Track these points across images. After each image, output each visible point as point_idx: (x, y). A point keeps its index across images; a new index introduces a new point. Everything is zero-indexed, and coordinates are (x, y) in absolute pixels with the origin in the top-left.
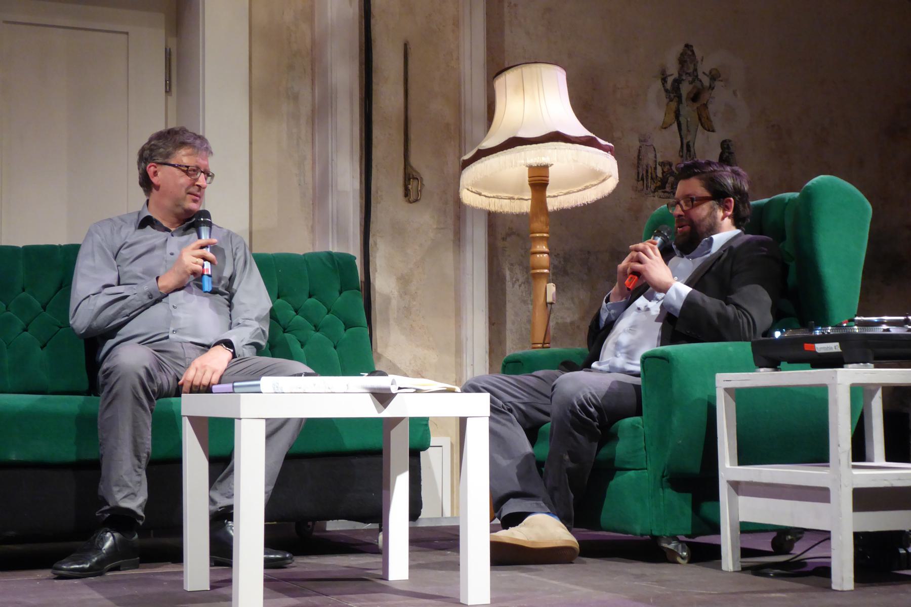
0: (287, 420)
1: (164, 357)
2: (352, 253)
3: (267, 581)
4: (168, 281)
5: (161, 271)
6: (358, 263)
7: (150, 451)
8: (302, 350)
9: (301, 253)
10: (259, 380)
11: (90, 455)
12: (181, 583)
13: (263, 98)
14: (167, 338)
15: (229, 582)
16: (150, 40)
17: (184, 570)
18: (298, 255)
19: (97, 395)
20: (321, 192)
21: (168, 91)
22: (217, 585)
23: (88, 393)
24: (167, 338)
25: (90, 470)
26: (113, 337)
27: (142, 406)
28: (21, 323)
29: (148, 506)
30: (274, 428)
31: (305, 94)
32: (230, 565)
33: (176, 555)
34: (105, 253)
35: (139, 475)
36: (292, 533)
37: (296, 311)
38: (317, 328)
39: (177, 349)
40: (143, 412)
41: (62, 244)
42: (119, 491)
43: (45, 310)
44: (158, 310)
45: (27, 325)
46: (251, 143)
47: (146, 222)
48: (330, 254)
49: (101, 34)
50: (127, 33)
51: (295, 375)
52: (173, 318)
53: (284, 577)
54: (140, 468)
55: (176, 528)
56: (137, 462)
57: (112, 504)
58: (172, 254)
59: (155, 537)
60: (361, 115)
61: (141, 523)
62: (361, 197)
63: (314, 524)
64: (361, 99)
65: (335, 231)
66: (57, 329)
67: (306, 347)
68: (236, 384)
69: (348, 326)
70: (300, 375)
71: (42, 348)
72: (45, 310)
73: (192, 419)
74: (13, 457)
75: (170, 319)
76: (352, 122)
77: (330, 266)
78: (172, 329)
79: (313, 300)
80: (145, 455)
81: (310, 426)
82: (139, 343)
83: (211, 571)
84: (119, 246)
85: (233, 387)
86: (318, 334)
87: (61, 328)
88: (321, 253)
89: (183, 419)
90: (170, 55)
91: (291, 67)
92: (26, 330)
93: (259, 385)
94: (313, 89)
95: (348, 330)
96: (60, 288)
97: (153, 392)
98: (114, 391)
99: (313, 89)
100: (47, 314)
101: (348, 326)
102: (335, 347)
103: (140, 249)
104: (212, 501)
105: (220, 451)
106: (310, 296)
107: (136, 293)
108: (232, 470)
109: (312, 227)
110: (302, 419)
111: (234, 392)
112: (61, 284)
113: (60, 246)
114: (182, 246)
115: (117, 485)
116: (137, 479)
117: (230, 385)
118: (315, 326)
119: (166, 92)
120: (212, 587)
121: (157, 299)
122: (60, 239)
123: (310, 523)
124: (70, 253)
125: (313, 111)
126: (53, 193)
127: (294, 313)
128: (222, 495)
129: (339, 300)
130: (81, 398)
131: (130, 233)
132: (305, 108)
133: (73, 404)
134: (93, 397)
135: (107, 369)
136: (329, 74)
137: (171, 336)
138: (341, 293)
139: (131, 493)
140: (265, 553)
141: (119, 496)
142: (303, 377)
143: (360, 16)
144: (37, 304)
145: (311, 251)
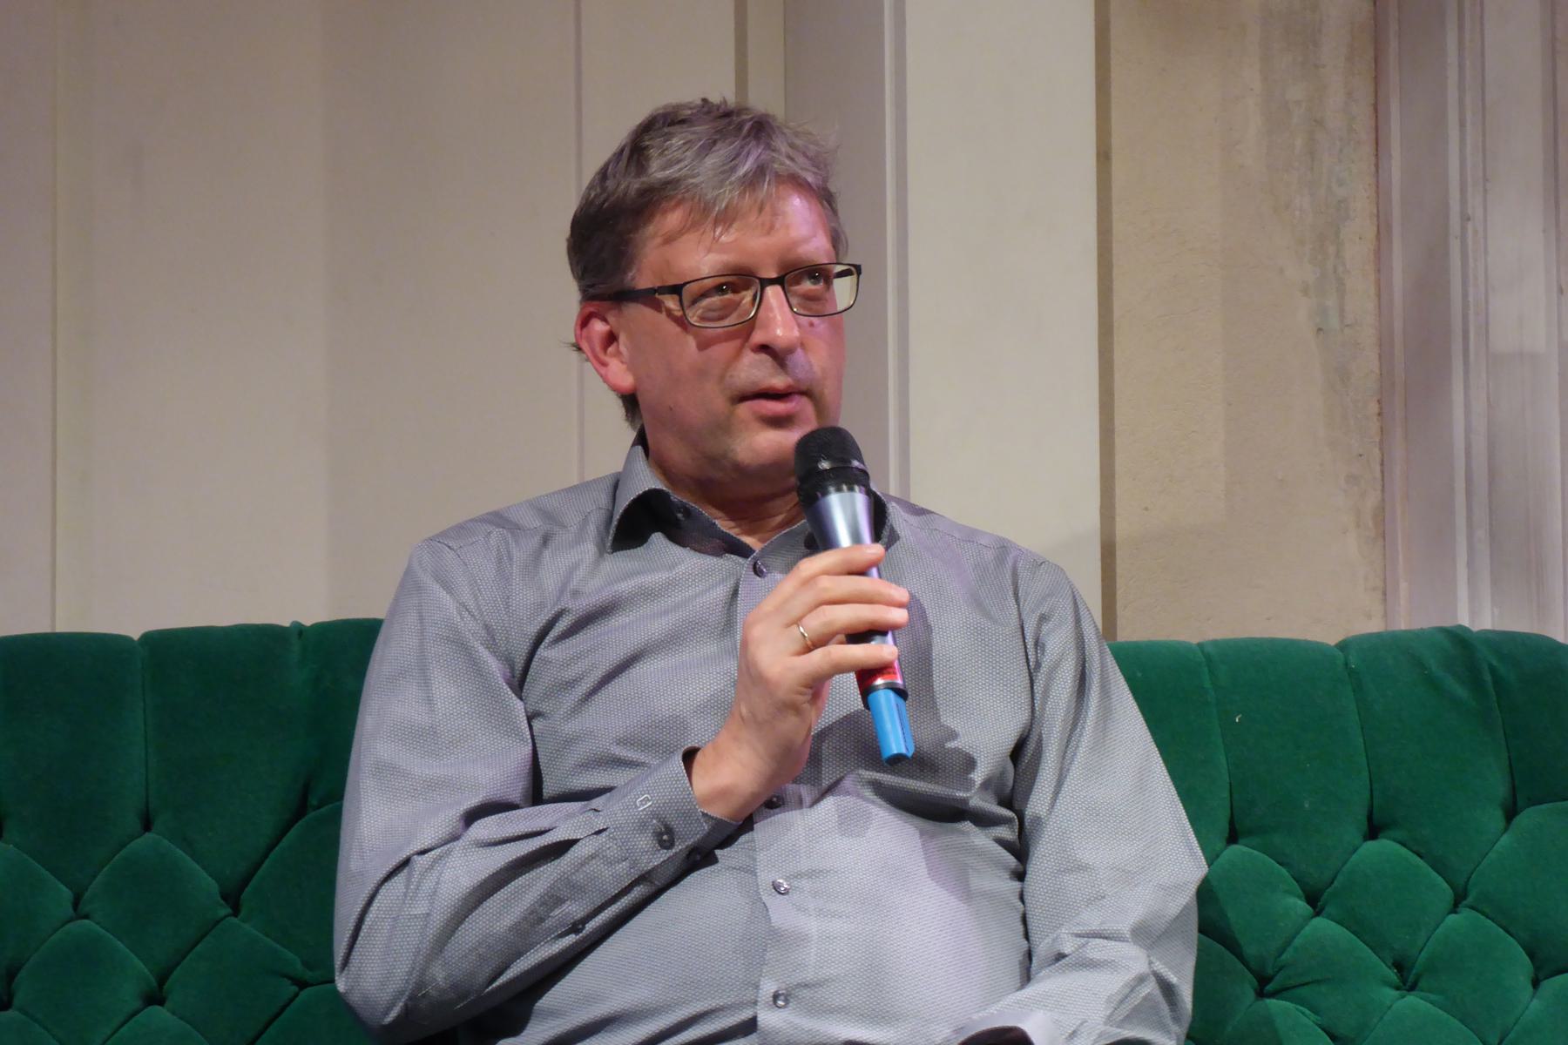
14: (749, 1027)
24: (749, 1027)
28: (137, 970)
37: (1314, 899)
38: (1406, 976)
41: (308, 621)
43: (236, 911)
45: (162, 979)
46: (1104, 156)
48: (1459, 639)
52: (777, 937)
65: (1481, 534)
66: (294, 988)
72: (236, 911)
75: (764, 941)
77: (1461, 691)
78: (768, 987)
79: (1384, 846)
86: (1412, 999)
87: (302, 985)
88: (1419, 635)
92: (154, 998)
96: (301, 811)
106: (1373, 832)
109: (1381, 517)
113: (299, 630)
118: (1400, 966)
121: (701, 848)
122: (298, 599)
124: (344, 652)
127: (1302, 906)
137: (769, 1019)
138: (1511, 813)
144: (209, 885)
145: (1374, 626)
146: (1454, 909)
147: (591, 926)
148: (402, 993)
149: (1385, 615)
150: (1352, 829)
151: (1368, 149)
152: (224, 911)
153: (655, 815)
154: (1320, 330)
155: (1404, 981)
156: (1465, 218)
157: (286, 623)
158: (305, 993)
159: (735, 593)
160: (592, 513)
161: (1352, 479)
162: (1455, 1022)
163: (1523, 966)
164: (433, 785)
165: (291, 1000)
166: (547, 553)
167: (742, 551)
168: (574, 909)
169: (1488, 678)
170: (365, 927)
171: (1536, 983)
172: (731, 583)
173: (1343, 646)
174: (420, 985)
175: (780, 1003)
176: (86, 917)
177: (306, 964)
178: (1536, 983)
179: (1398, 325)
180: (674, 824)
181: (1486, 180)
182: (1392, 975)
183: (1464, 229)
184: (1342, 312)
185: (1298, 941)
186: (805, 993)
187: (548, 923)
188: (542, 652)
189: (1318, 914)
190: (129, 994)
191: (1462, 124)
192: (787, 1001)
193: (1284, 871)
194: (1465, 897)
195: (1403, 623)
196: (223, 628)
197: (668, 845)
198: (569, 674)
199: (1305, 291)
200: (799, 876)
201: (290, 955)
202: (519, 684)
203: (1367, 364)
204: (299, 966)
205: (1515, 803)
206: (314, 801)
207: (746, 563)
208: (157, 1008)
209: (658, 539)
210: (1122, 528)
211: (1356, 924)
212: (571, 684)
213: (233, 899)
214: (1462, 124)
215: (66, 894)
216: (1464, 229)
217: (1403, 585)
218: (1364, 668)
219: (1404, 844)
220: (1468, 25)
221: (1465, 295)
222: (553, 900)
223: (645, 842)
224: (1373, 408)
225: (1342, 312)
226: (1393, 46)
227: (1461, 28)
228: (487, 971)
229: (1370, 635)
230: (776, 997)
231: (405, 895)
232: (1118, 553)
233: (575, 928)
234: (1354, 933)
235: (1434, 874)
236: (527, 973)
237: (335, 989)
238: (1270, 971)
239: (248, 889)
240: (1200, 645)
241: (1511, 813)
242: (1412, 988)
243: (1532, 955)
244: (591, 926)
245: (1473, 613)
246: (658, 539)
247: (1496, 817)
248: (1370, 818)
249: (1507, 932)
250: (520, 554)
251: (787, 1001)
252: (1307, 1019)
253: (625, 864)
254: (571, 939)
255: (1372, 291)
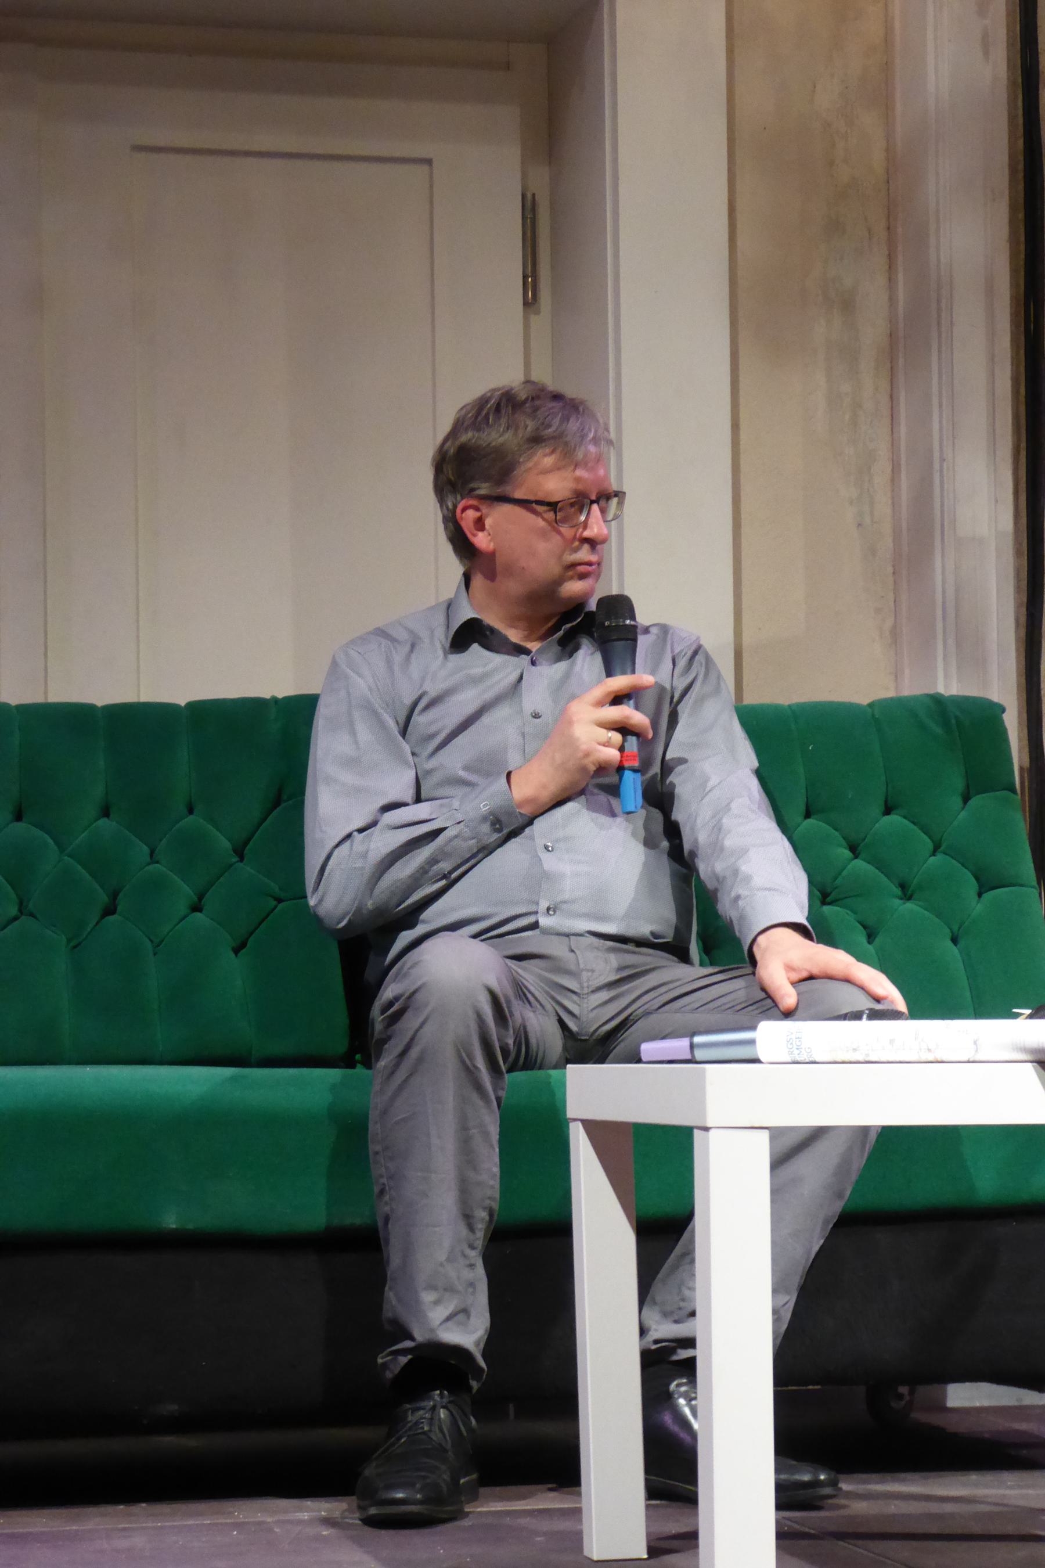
0: (818, 1134)
1: (530, 974)
2: (995, 698)
3: (784, 1536)
4: (532, 783)
5: (513, 760)
6: (1013, 722)
7: (496, 1206)
8: (870, 947)
9: (864, 700)
10: (753, 1028)
11: (354, 1217)
12: (576, 1540)
13: (765, 310)
14: (535, 926)
15: (690, 1539)
16: (480, 173)
17: (584, 1505)
18: (858, 706)
19: (368, 1064)
20: (914, 542)
21: (530, 303)
22: (665, 1544)
23: (347, 1062)
24: (535, 926)
25: (358, 1254)
26: (411, 926)
27: (479, 1087)
28: (186, 892)
29: (493, 1342)
30: (791, 1149)
31: (873, 293)
32: (691, 1500)
33: (561, 1468)
34: (375, 713)
35: (472, 1266)
36: (841, 1415)
37: (854, 849)
38: (906, 892)
39: (556, 948)
40: (480, 1103)
41: (280, 696)
42: (437, 1302)
43: (242, 858)
44: (511, 856)
45: (201, 897)
46: (735, 426)
47: (468, 635)
48: (938, 702)
49: (363, 166)
50: (429, 162)
51: (844, 1017)
52: (547, 876)
53: (832, 1528)
54: (472, 1247)
55: (562, 1399)
56: (464, 1231)
57: (420, 1336)
58: (536, 716)
59: (517, 1420)
60: (1014, 341)
61: (475, 1385)
62: (1018, 553)
63: (912, 1392)
64: (1014, 298)
65: (951, 641)
66: (274, 903)
67: (878, 941)
68: (697, 1039)
69: (985, 884)
70: (857, 1016)
71: (237, 951)
72: (242, 858)
73: (596, 1129)
74: (171, 1221)
75: (539, 879)
76: (992, 359)
77: (939, 730)
78: (544, 905)
79: (894, 818)
80: (484, 1215)
81: (894, 1145)
82: (475, 936)
83: (647, 1507)
84: (408, 701)
85: (692, 1046)
86: (909, 905)
87: (280, 901)
88: (915, 699)
89: (572, 1125)
90: (534, 209)
91: (835, 227)
92: (196, 908)
93: (752, 1042)
94: (891, 280)
95: (988, 896)
96: (277, 803)
97: (505, 1051)
98: (414, 1053)
99: (891, 280)
100: (246, 870)
101: (985, 884)
102: (955, 940)
103: (466, 702)
104: (643, 1331)
105: (661, 1206)
106: (888, 811)
107: (458, 814)
108: (689, 1255)
109: (895, 634)
110: (865, 1130)
111: (692, 1061)
112: (280, 792)
113: (275, 700)
114: (563, 693)
115: (432, 1287)
116: (467, 1274)
117: (685, 1042)
118: (903, 886)
119: (526, 304)
120: (654, 1551)
121: (509, 826)
122: (275, 683)
123: (904, 1390)
124: (300, 712)
125: (892, 335)
126: (234, 573)
127: (847, 853)
128: (666, 1315)
129: (960, 818)
130: (334, 1074)
131: (435, 668)
132: (872, 330)
133: (312, 1088)
134: (360, 1070)
135: (397, 999)
136: (932, 241)
137: (544, 921)
138: (966, 799)
139: (451, 1309)
140: (777, 1470)
141: (437, 1315)
142: (865, 1023)
143: (1012, 83)
144: (224, 844)
145: (891, 694)
146: (934, 853)
147: (454, 876)
148: (347, 913)
149: (896, 688)
150: (877, 808)
151: (887, 421)
152: (235, 859)
153: (491, 813)
154: (859, 525)
155: (905, 894)
156: (942, 460)
157: (268, 696)
158: (281, 906)
159: (521, 678)
160: (441, 637)
161: (878, 611)
162: (932, 916)
163: (973, 885)
164: (358, 790)
165: (274, 909)
166: (413, 656)
167: (526, 652)
168: (445, 866)
169: (953, 721)
170: (326, 873)
171: (980, 895)
172: (519, 672)
173: (871, 705)
174: (359, 910)
175: (551, 912)
176: (157, 862)
177: (280, 889)
178: (980, 895)
179: (904, 525)
180: (503, 819)
181: (954, 438)
182: (898, 891)
183: (941, 467)
184: (872, 513)
185: (845, 873)
186: (564, 906)
187: (431, 873)
188: (415, 718)
189: (856, 857)
190: (182, 907)
191: (940, 406)
192: (555, 911)
193: (836, 833)
194: (940, 847)
195: (906, 692)
196: (233, 700)
197: (499, 831)
198: (433, 729)
199: (851, 503)
200: (557, 841)
201: (272, 884)
202: (404, 733)
203: (887, 543)
204: (277, 889)
205: (969, 793)
206: (285, 797)
207: (525, 659)
208: (198, 914)
209: (475, 646)
210: (747, 639)
211: (880, 865)
212: (432, 736)
213: (240, 853)
214: (940, 406)
215: (146, 849)
216: (941, 467)
217: (907, 671)
218: (883, 717)
219: (905, 817)
220: (944, 336)
221: (942, 505)
222: (433, 861)
223: (486, 828)
224: (890, 569)
225: (872, 513)
226: (901, 361)
227: (940, 352)
228: (395, 900)
229: (886, 700)
230: (548, 909)
231: (349, 856)
232: (744, 655)
233: (444, 877)
234: (877, 868)
235: (922, 834)
236: (417, 902)
237: (307, 905)
238: (829, 890)
239: (248, 847)
240: (789, 706)
241: (966, 799)
242: (910, 898)
243: (977, 879)
244: (454, 876)
245: (946, 686)
246: (475, 646)
247: (958, 801)
248: (886, 802)
249: (963, 865)
250: (398, 658)
251: (555, 911)
252: (850, 918)
253: (474, 841)
254: (443, 882)
255: (890, 502)
